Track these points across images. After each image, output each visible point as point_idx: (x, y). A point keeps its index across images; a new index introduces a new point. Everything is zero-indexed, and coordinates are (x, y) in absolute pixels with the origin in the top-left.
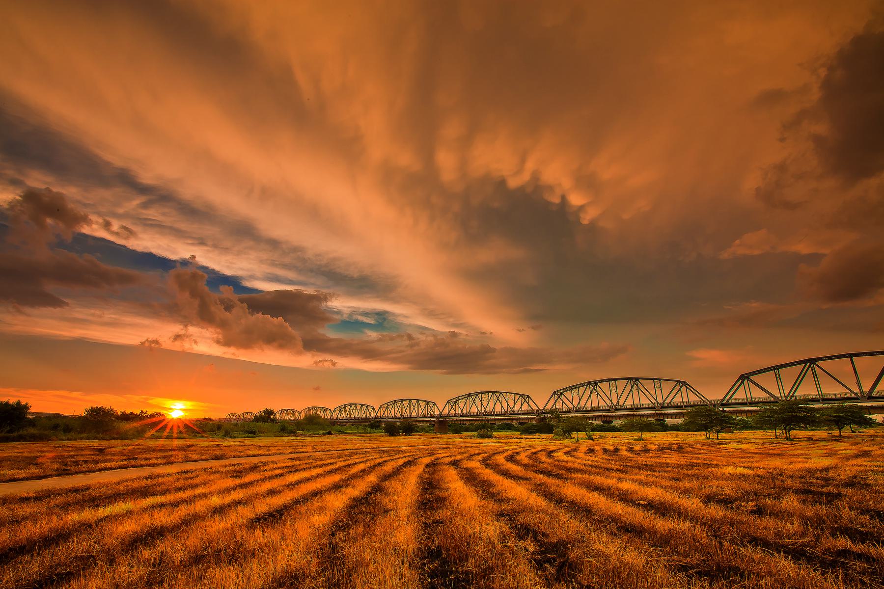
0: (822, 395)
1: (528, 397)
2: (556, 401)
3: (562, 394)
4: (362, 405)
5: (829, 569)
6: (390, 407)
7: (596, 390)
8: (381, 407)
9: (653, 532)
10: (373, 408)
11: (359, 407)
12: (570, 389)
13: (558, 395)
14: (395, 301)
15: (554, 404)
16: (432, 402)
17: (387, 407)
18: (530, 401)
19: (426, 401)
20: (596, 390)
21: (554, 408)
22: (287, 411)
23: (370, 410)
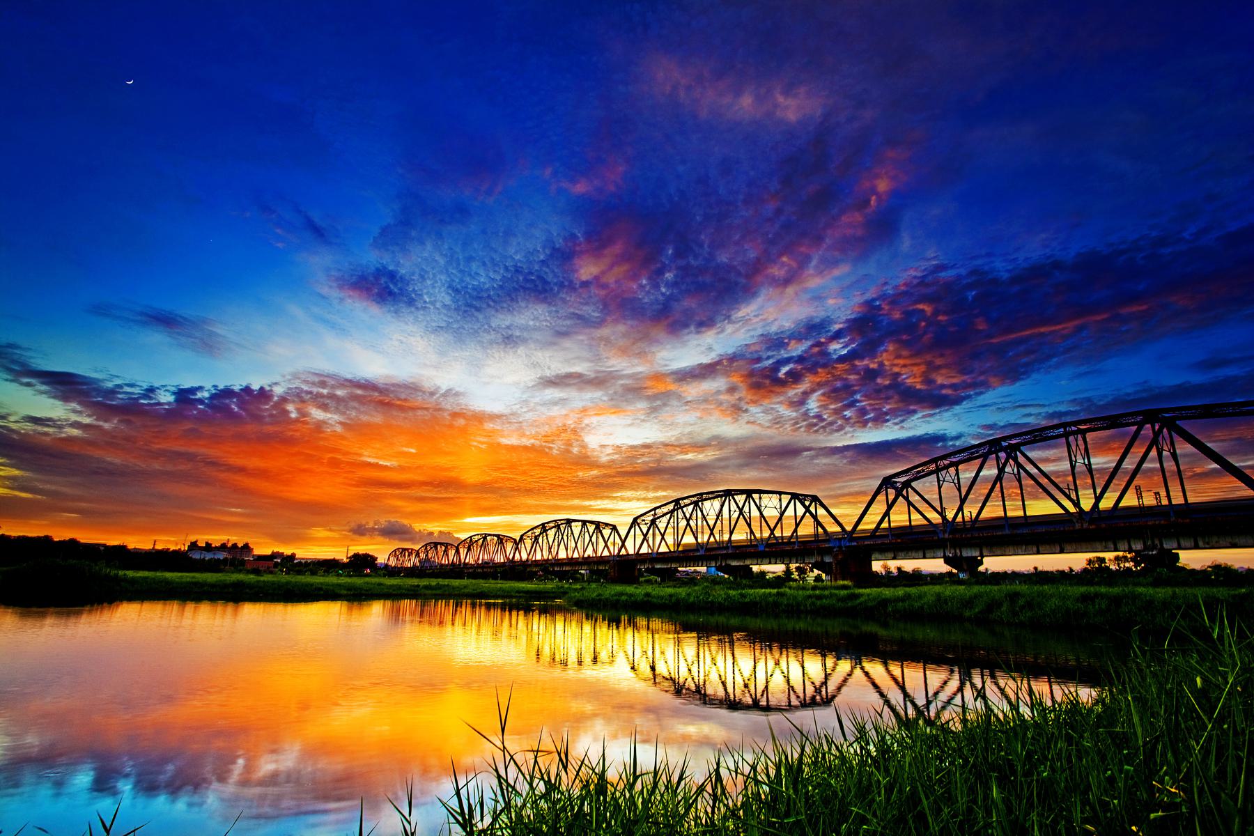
0: (1069, 446)
1: (815, 499)
2: (890, 507)
3: (907, 485)
4: (584, 523)
5: (852, 811)
6: (662, 524)
7: (907, 498)
8: (635, 522)
9: (649, 779)
10: (614, 528)
11: (576, 528)
12: (933, 467)
13: (896, 489)
14: (1198, 601)
15: (887, 514)
16: (607, 525)
17: (653, 522)
18: (821, 511)
19: (498, 536)
20: (907, 498)
21: (885, 525)
22: (485, 538)
23: (606, 532)
